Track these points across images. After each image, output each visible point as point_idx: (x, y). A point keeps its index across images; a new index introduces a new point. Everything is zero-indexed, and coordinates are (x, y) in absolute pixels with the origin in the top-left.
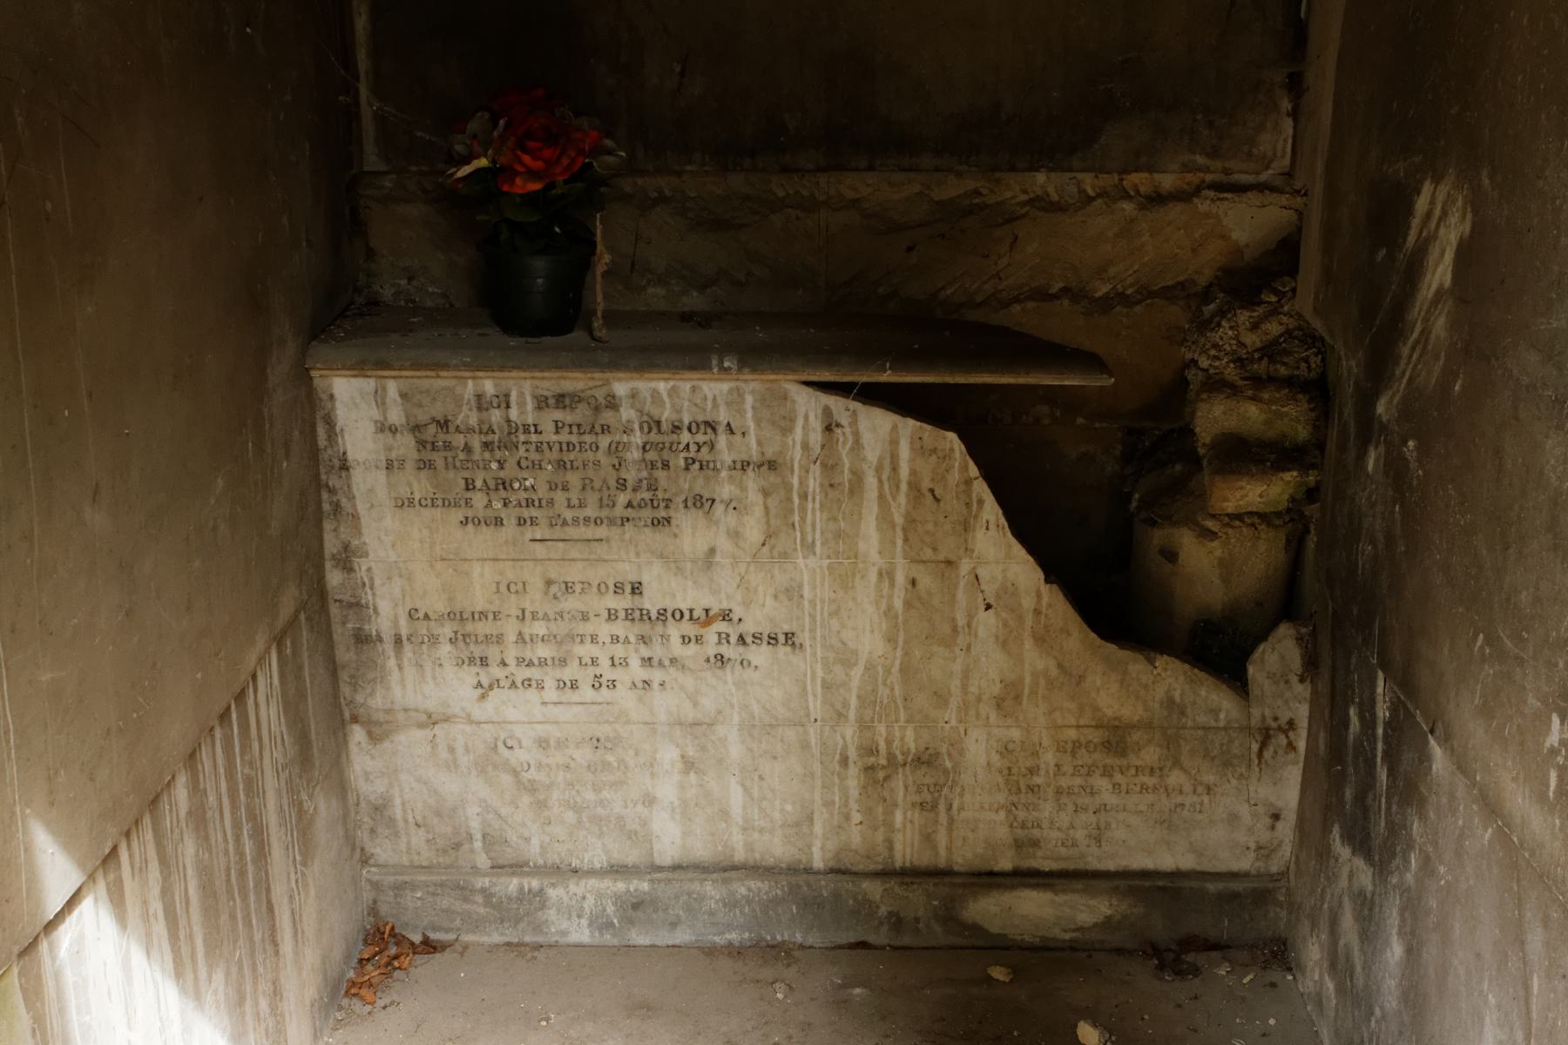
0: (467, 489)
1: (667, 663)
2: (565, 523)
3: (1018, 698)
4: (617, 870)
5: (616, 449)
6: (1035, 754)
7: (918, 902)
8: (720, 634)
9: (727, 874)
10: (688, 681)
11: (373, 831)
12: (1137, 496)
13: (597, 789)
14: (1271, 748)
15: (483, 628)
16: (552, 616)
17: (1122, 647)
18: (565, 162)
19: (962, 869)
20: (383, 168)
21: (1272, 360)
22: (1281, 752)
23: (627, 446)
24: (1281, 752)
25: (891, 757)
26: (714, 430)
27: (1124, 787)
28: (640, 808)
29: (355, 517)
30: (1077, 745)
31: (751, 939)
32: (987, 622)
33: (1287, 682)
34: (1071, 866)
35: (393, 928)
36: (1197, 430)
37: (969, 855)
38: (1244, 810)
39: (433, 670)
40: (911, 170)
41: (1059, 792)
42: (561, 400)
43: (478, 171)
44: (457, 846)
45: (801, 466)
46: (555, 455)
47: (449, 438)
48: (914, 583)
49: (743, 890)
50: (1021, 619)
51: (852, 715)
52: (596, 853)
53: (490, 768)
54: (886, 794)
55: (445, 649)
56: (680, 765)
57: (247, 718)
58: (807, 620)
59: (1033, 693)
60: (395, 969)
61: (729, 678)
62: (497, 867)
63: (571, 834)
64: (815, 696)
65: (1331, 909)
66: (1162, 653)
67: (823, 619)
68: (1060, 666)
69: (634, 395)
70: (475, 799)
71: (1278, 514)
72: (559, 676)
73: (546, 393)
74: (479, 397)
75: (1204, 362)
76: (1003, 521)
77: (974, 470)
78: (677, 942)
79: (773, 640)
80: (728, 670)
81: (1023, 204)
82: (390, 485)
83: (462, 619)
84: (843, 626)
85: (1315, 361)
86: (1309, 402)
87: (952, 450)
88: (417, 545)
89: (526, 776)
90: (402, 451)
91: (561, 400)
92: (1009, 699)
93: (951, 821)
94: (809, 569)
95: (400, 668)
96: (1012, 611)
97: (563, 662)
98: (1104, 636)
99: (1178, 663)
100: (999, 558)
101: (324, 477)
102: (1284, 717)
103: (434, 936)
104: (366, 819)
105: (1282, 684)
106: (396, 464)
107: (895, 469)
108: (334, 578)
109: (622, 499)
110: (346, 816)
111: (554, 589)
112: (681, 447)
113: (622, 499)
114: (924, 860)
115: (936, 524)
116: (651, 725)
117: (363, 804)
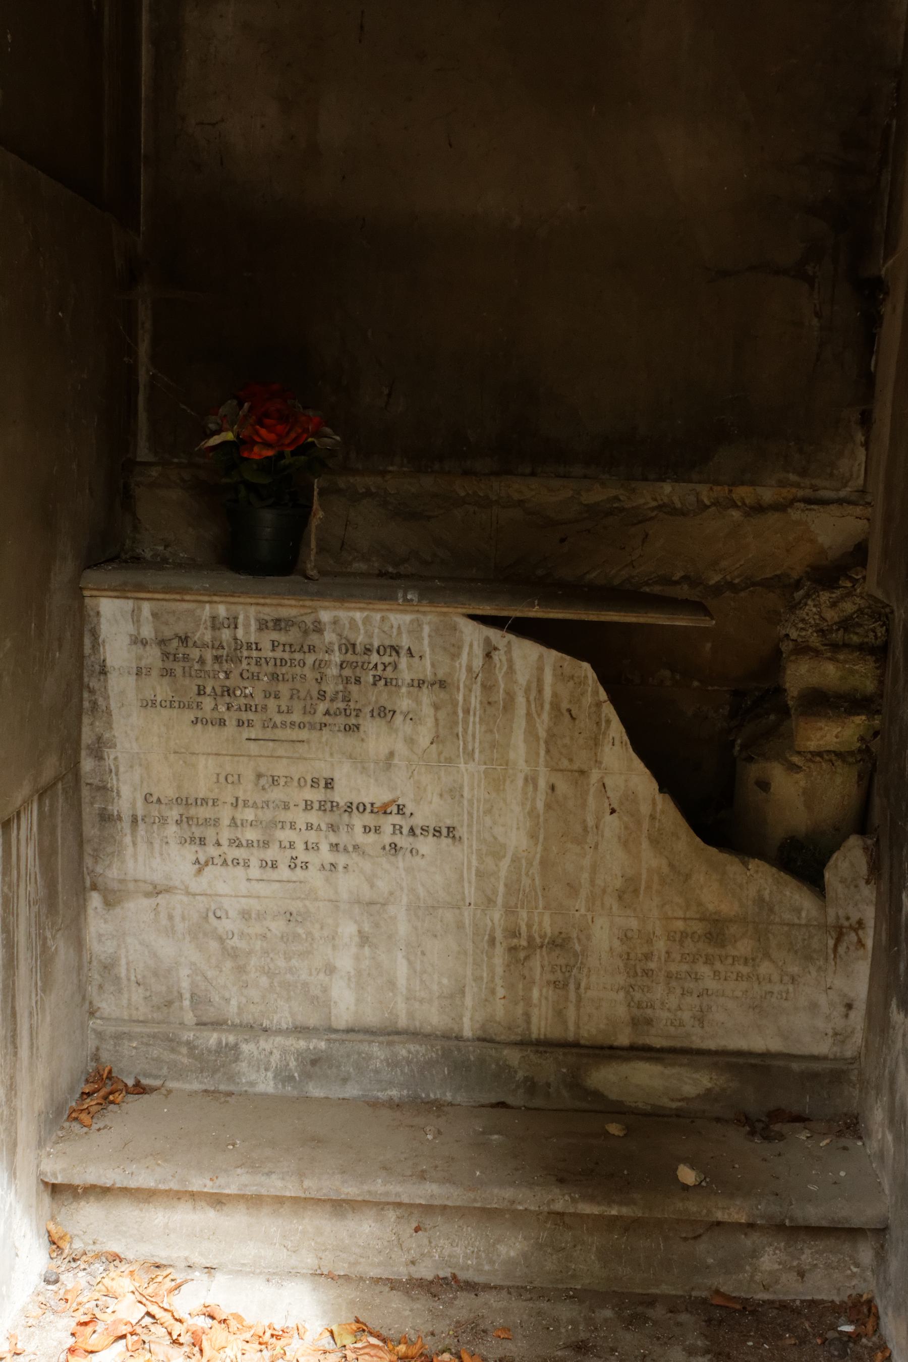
0: (199, 694)
1: (350, 849)
2: (275, 726)
3: (636, 891)
4: (301, 1030)
5: (319, 666)
6: (649, 942)
7: (549, 1069)
8: (394, 825)
9: (391, 1038)
10: (367, 866)
11: (101, 987)
12: (739, 741)
13: (288, 958)
14: (845, 945)
15: (203, 812)
16: (260, 805)
17: (720, 851)
18: (293, 435)
19: (587, 1043)
20: (151, 458)
21: (846, 630)
22: (852, 948)
23: (328, 663)
24: (852, 948)
25: (530, 939)
26: (398, 653)
27: (723, 975)
28: (322, 976)
29: (109, 714)
30: (684, 935)
31: (409, 1096)
32: (611, 824)
33: (856, 886)
34: (678, 1044)
35: (110, 1072)
36: (787, 685)
37: (594, 1031)
38: (822, 1000)
39: (161, 846)
40: (565, 477)
41: (669, 976)
42: (278, 624)
43: (225, 443)
44: (169, 1004)
45: (465, 686)
46: (270, 669)
47: (187, 651)
48: (553, 788)
49: (404, 1052)
50: (639, 823)
51: (500, 900)
52: (283, 1016)
53: (201, 935)
54: (526, 972)
55: (172, 830)
56: (357, 939)
57: (10, 848)
58: (466, 817)
59: (648, 888)
60: (112, 1102)
61: (401, 865)
62: (201, 1024)
63: (264, 997)
64: (470, 882)
65: (890, 1073)
66: (754, 858)
67: (478, 816)
68: (671, 865)
69: (335, 622)
70: (187, 962)
71: (851, 753)
72: (262, 856)
73: (266, 617)
74: (214, 618)
75: (794, 634)
76: (626, 738)
77: (603, 695)
78: (347, 1095)
79: (437, 832)
80: (400, 857)
81: (653, 509)
82: (139, 689)
83: (187, 804)
84: (495, 823)
85: (880, 631)
86: (875, 662)
87: (586, 677)
88: (156, 739)
89: (230, 943)
90: (149, 660)
91: (278, 624)
92: (629, 892)
93: (579, 999)
94: (469, 772)
95: (134, 844)
96: (632, 815)
97: (266, 844)
98: (708, 840)
99: (767, 866)
100: (622, 770)
101: (86, 680)
102: (855, 917)
103: (145, 1081)
104: (96, 976)
105: (852, 888)
106: (144, 671)
107: (540, 691)
108: (87, 764)
109: (322, 707)
110: (80, 968)
111: (263, 781)
112: (371, 666)
113: (322, 707)
114: (556, 1033)
115: (572, 738)
116: (334, 903)
117: (95, 963)
